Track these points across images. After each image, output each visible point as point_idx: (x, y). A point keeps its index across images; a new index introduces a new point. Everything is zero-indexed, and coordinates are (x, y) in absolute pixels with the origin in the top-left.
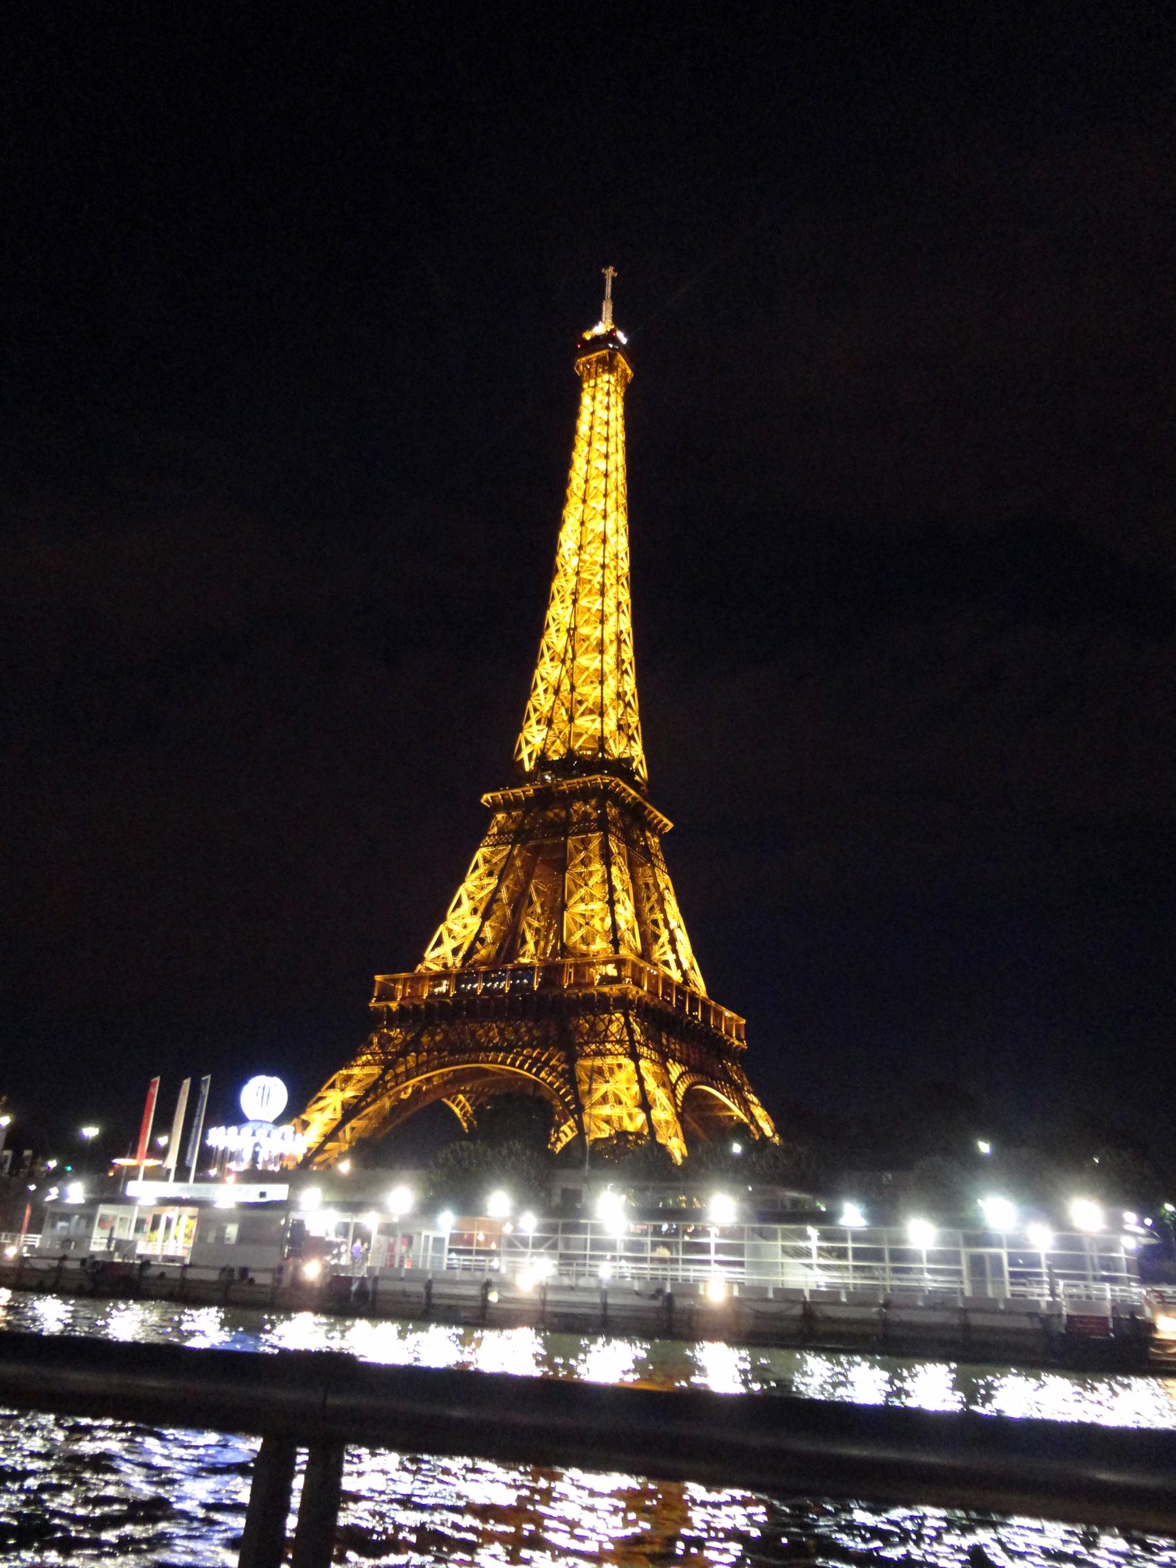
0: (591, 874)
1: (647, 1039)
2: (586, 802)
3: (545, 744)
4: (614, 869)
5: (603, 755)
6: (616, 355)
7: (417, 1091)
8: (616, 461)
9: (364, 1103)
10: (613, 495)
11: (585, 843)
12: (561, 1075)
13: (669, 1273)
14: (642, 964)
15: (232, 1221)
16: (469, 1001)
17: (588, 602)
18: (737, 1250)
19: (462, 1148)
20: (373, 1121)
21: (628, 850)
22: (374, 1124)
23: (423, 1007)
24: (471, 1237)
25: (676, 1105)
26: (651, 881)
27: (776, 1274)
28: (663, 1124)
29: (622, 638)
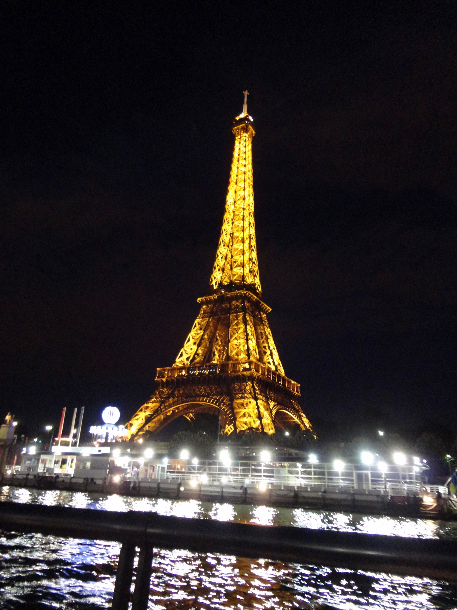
0: (239, 329)
1: (261, 392)
2: (237, 301)
3: (222, 278)
7: (173, 412)
9: (153, 417)
10: (248, 181)
11: (237, 317)
12: (228, 406)
14: (259, 363)
15: (88, 461)
17: (238, 223)
19: (182, 433)
22: (157, 425)
23: (175, 380)
24: (175, 466)
25: (272, 417)
26: (263, 331)
27: (285, 480)
28: (267, 425)
29: (251, 237)
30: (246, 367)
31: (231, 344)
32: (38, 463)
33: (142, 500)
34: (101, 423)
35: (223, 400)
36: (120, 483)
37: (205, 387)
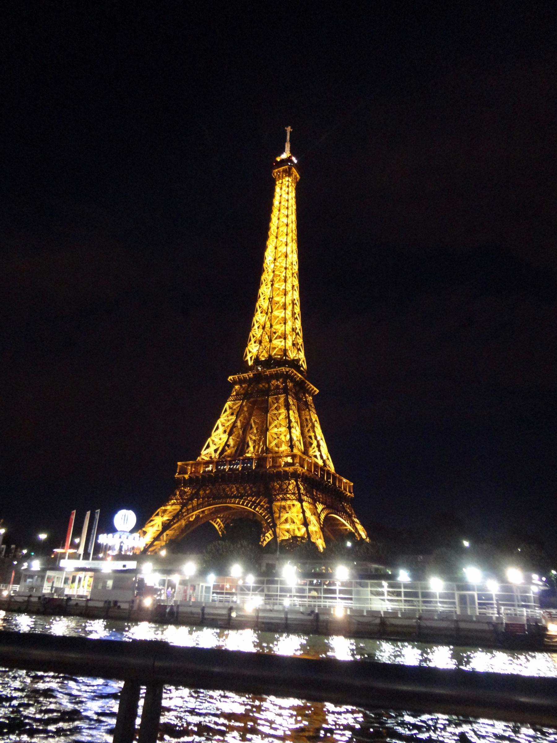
0: (280, 414)
1: (307, 492)
2: (278, 380)
3: (258, 352)
4: (291, 412)
5: (286, 358)
6: (292, 168)
7: (198, 517)
8: (292, 219)
9: (172, 523)
10: (290, 235)
11: (277, 399)
12: (266, 509)
13: (317, 603)
14: (304, 457)
15: (110, 579)
16: (222, 474)
17: (279, 285)
18: (349, 592)
19: (219, 544)
20: (177, 531)
21: (297, 403)
22: (177, 532)
23: (200, 477)
24: (223, 586)
25: (320, 524)
26: (308, 418)
27: (368, 604)
28: (314, 533)
29: (295, 302)
34: (110, 529)
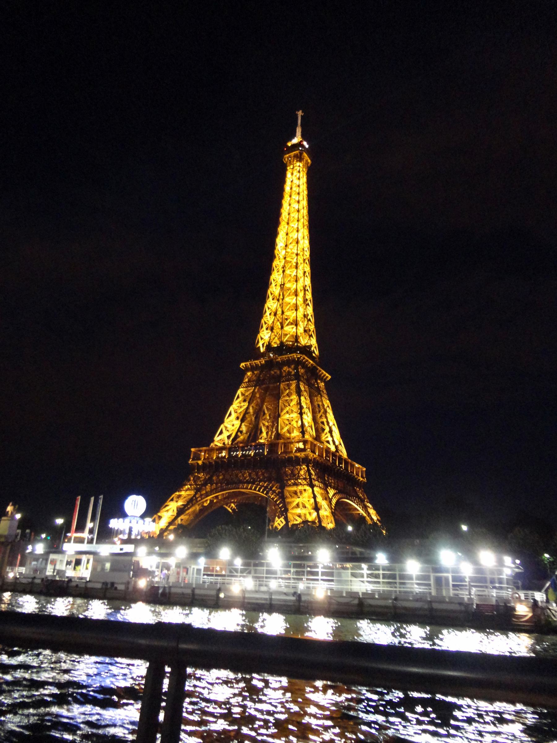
0: (292, 400)
1: (318, 478)
2: (289, 367)
3: (270, 339)
7: (211, 501)
9: (186, 508)
10: (302, 220)
11: (289, 386)
12: (278, 494)
14: (316, 442)
15: (108, 561)
17: (291, 272)
18: (331, 574)
19: (221, 527)
22: (192, 517)
23: (213, 463)
24: (213, 568)
25: (331, 508)
26: (320, 404)
27: (348, 585)
28: (325, 517)
29: (306, 288)
30: (300, 447)
31: (282, 419)
32: (46, 564)
33: (173, 609)
34: (124, 515)
35: (271, 488)
36: (147, 588)
37: (250, 472)
